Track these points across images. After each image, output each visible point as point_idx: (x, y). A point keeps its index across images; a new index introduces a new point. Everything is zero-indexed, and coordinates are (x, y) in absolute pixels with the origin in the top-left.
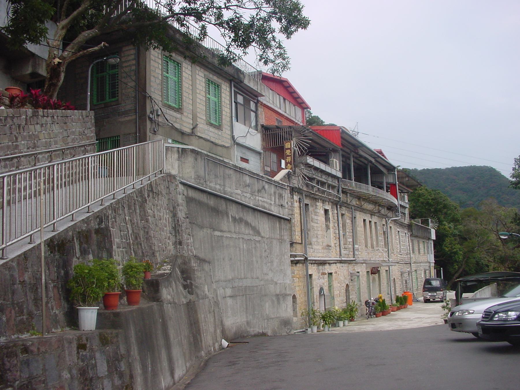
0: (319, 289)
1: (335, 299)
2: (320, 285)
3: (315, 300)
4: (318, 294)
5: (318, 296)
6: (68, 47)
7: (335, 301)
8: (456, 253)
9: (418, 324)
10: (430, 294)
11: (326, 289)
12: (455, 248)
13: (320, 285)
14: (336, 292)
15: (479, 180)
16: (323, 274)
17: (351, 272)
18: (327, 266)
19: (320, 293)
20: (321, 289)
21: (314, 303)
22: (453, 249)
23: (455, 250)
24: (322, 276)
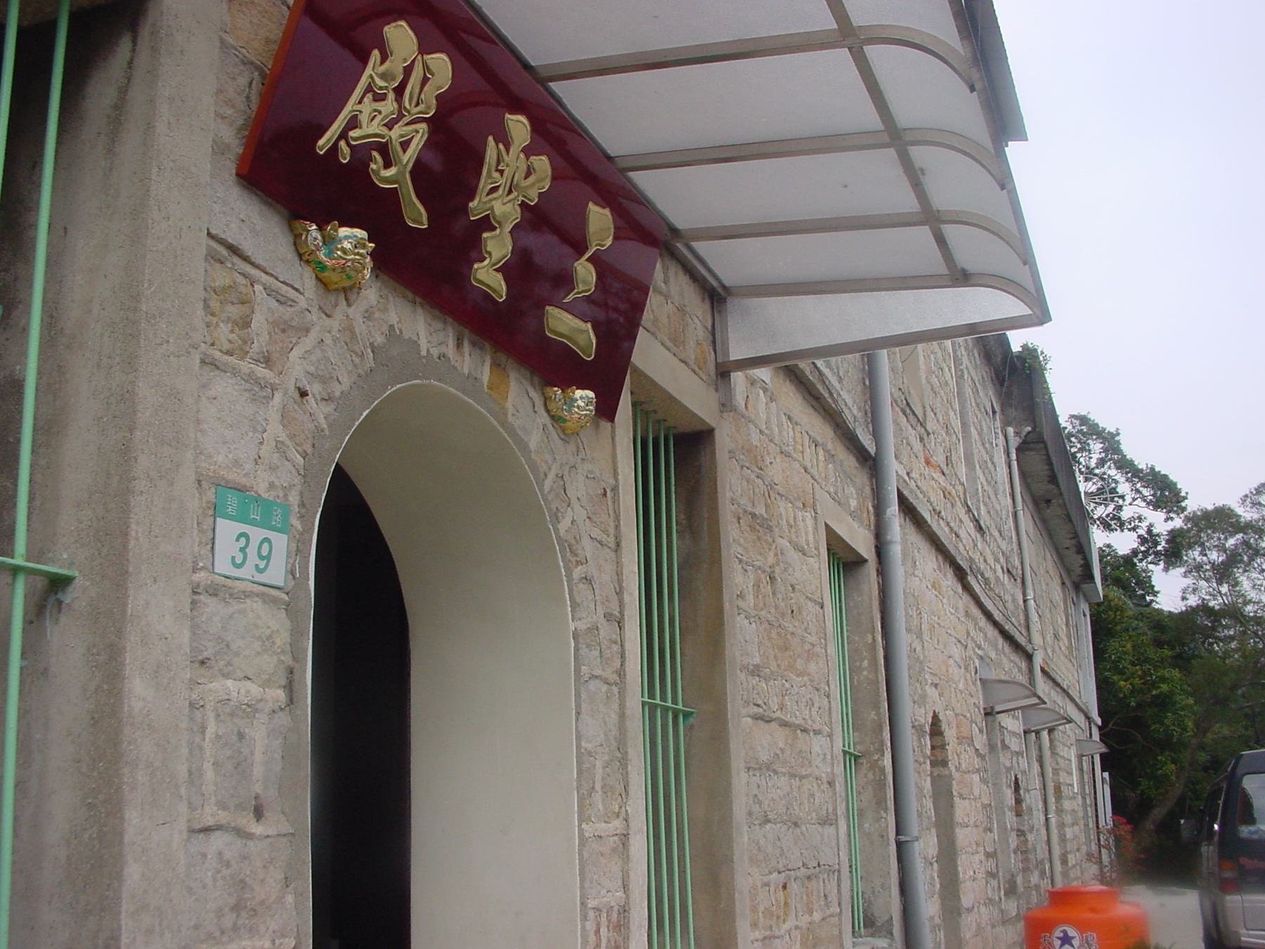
8: (1163, 703)
12: (1163, 679)
22: (1154, 685)
23: (1165, 687)
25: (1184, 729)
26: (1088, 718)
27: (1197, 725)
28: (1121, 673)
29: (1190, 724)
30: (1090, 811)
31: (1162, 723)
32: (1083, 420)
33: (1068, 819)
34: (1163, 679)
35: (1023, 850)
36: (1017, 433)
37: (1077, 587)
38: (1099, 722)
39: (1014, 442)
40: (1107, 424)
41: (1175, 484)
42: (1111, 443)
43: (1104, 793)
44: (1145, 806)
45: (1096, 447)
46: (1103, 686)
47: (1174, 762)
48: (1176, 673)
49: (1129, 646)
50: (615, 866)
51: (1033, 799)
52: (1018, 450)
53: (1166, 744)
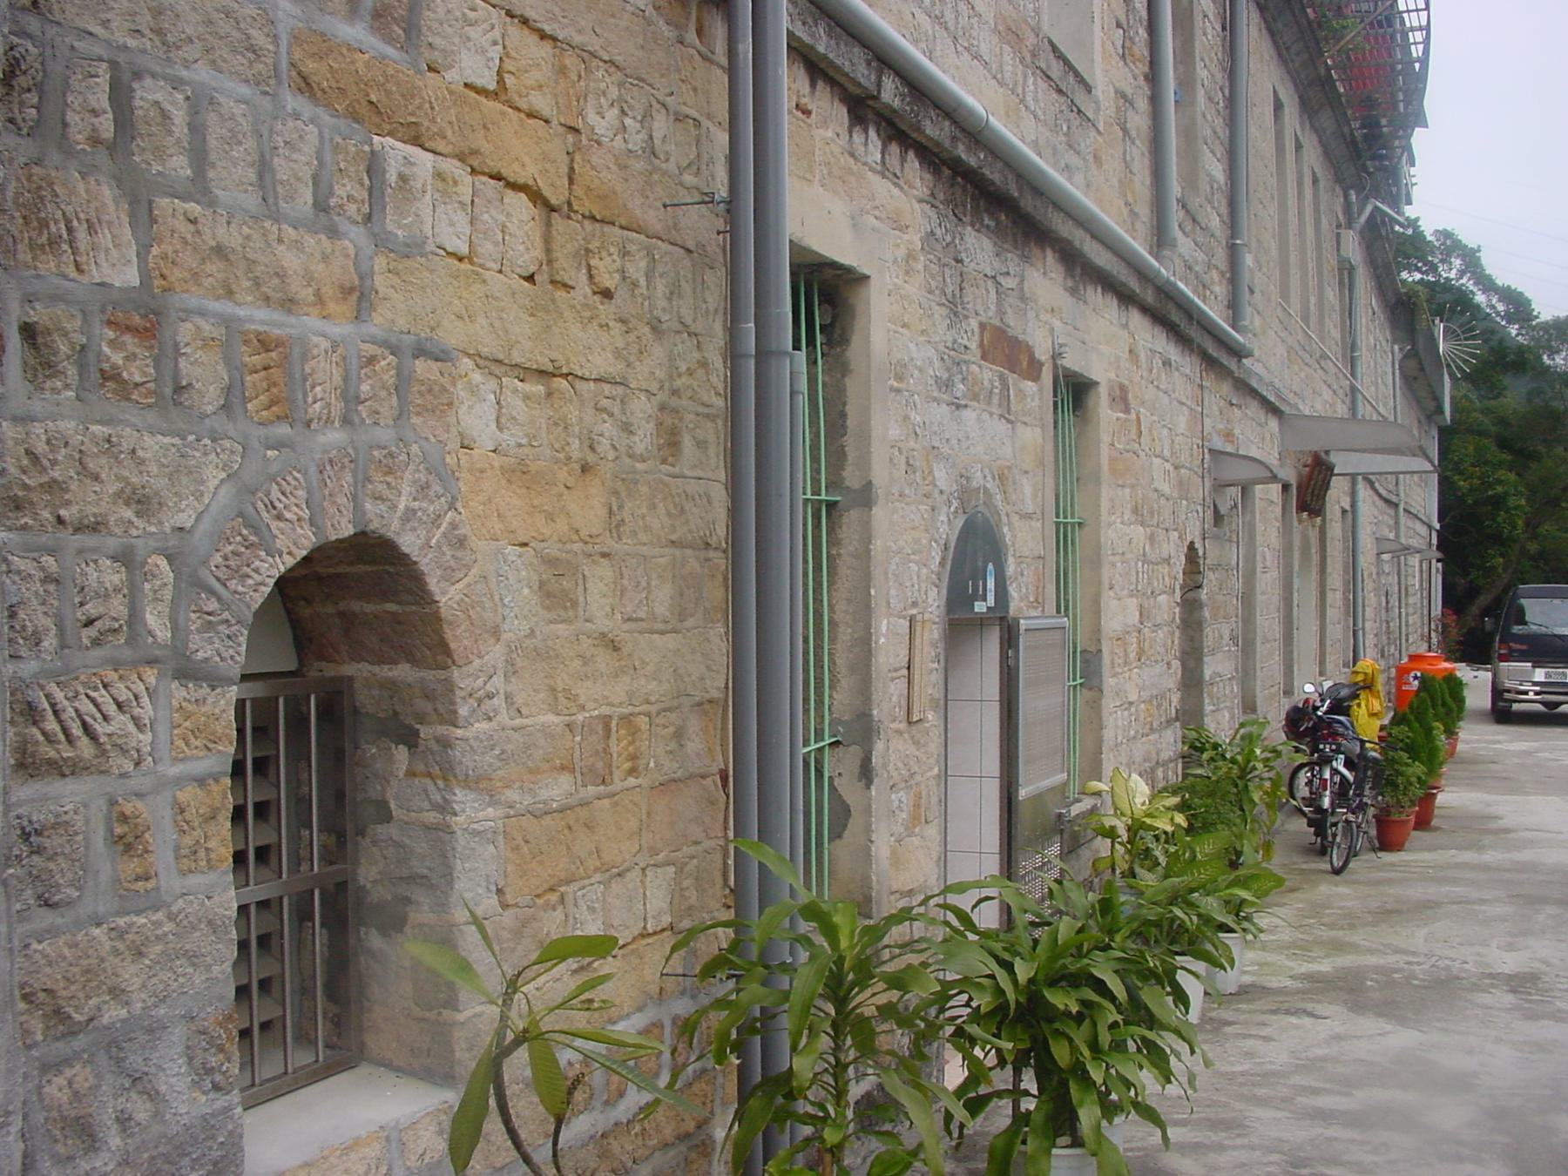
0: (948, 527)
1: (1109, 682)
2: (965, 494)
3: (888, 698)
4: (934, 603)
5: (932, 635)
6: (346, 534)
7: (1109, 703)
8: (1498, 502)
9: (1313, 866)
10: (1540, 675)
11: (1025, 540)
12: (1500, 482)
13: (965, 494)
14: (1119, 614)
15: (239, 1164)
16: (1007, 350)
17: (1218, 443)
18: (1044, 281)
19: (959, 596)
20: (975, 550)
21: (863, 730)
22: (1491, 486)
23: (1499, 489)
24: (988, 374)
25: (1515, 528)
26: (1430, 527)
27: (1527, 524)
28: (1461, 473)
29: (1520, 522)
30: (1426, 602)
31: (1494, 519)
32: (1446, 234)
33: (1411, 610)
34: (1500, 482)
35: (1388, 632)
36: (1401, 350)
37: (1429, 417)
38: (1438, 526)
39: (1398, 356)
40: (1468, 238)
41: (1529, 302)
42: (1471, 261)
43: (1437, 581)
44: (1473, 592)
45: (1457, 262)
46: (1445, 486)
47: (1502, 555)
48: (1512, 477)
49: (1471, 448)
50: (838, 617)
51: (1394, 602)
52: (1401, 361)
53: (1497, 539)
